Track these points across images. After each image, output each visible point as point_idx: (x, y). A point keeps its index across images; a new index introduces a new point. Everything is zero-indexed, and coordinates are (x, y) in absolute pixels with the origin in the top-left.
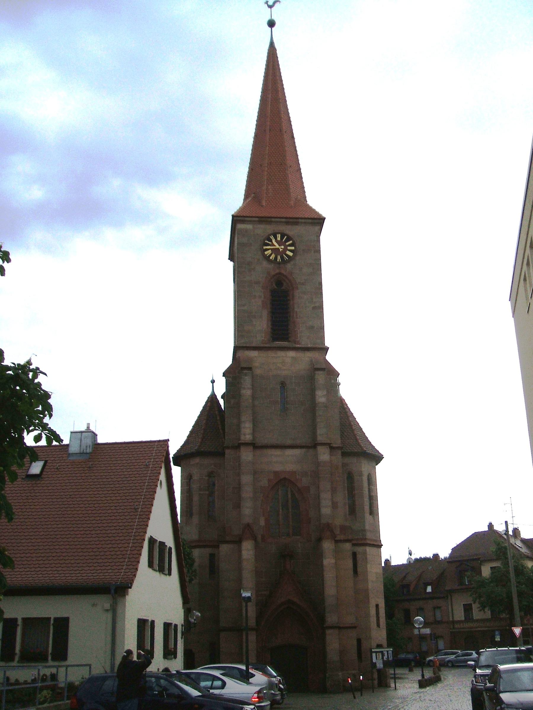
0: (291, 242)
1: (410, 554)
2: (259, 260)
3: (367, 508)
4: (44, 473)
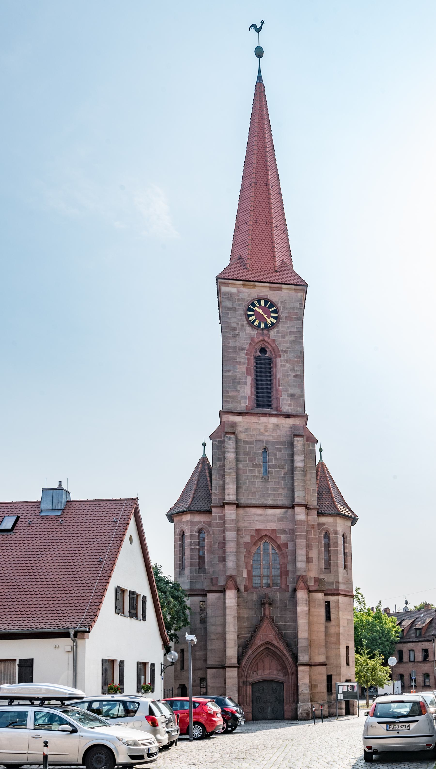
0: (274, 308)
1: (406, 603)
3: (341, 562)
4: (16, 528)
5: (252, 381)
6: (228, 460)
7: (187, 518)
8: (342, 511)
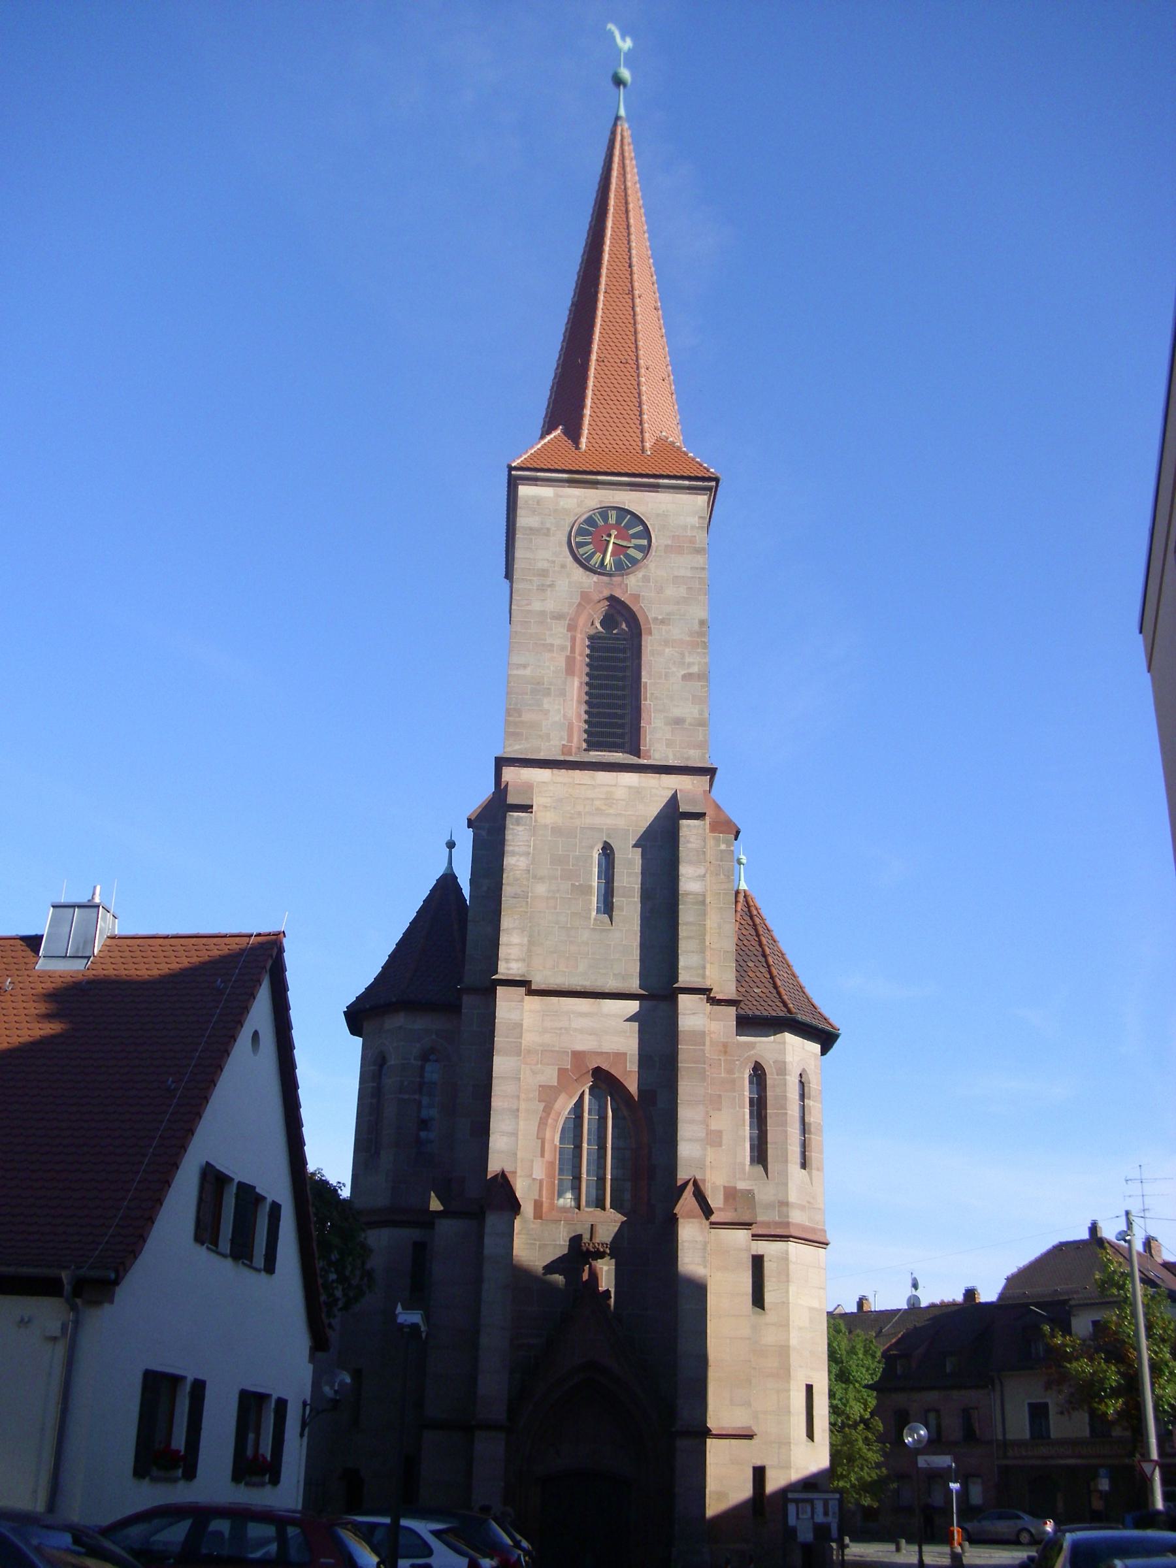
1: (915, 1286)
2: (563, 566)
5: (580, 688)
6: (511, 874)
7: (397, 1021)
8: (798, 1011)
